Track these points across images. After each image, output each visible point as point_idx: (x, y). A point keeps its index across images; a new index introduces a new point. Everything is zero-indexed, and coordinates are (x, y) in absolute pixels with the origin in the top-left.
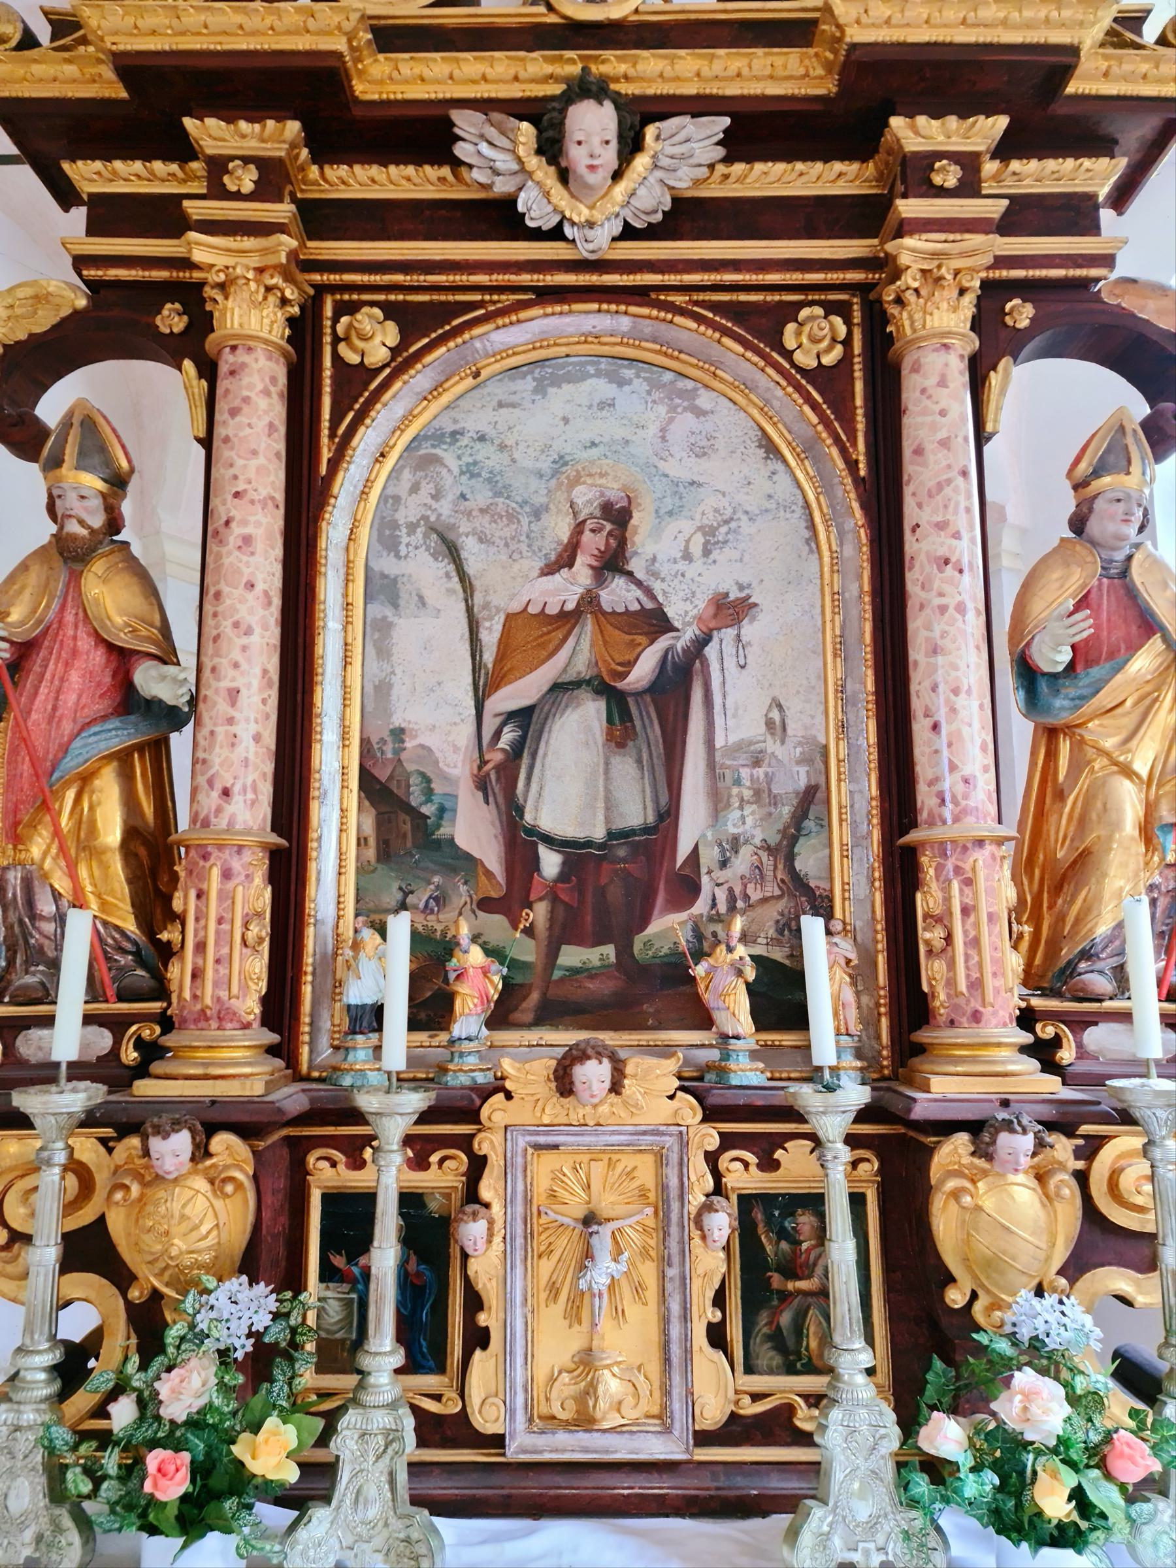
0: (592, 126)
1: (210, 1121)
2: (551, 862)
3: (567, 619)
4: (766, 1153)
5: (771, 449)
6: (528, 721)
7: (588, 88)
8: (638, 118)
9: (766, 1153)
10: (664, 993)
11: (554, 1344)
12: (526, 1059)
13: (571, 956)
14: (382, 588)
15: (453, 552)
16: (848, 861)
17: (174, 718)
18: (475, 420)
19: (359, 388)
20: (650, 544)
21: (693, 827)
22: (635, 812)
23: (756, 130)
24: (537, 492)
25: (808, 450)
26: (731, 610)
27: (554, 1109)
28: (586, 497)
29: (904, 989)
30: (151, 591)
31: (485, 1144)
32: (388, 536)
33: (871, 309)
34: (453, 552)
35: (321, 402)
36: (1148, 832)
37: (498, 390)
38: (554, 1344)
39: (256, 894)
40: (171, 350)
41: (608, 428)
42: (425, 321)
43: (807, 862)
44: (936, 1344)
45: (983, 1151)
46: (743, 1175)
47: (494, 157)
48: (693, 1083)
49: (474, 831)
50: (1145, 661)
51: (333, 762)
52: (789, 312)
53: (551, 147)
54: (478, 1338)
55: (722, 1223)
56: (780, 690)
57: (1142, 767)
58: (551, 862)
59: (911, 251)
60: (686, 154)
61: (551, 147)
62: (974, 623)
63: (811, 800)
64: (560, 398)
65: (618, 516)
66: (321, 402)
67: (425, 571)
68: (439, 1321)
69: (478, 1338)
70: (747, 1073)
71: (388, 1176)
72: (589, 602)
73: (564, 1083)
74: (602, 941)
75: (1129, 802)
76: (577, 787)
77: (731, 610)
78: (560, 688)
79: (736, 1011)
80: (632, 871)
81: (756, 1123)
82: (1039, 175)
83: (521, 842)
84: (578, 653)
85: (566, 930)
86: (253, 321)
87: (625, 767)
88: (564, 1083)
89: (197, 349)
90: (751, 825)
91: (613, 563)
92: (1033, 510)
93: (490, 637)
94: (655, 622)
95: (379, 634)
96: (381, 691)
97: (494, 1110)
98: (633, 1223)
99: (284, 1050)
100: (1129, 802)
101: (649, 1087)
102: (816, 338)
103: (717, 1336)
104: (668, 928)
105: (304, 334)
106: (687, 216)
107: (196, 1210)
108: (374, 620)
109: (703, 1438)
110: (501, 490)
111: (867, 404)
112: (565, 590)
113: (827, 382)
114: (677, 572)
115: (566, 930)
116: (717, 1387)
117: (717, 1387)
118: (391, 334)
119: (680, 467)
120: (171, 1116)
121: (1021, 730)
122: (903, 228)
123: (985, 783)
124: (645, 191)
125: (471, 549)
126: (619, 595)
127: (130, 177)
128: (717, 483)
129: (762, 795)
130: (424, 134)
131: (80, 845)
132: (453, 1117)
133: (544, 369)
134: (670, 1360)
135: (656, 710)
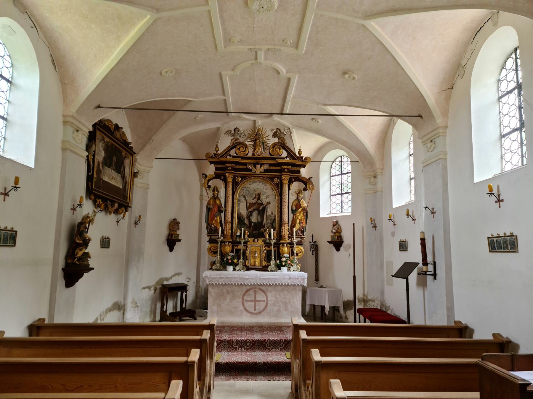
0: (258, 166)
1: (229, 242)
2: (253, 224)
3: (255, 204)
4: (269, 247)
5: (272, 189)
6: (251, 213)
7: (258, 164)
8: (261, 165)
9: (269, 247)
10: (262, 235)
11: (252, 261)
12: (251, 240)
13: (254, 232)
14: (239, 200)
15: (245, 197)
16: (277, 226)
17: (222, 212)
18: (247, 186)
19: (237, 183)
20: (263, 197)
21: (265, 222)
22: (260, 220)
23: (271, 165)
24: (252, 192)
25: (275, 190)
26: (269, 203)
27: (253, 243)
28: (256, 193)
29: (109, 135)
30: (220, 201)
31: (248, 245)
32: (239, 196)
33: (280, 178)
34: (245, 197)
35: (235, 185)
36: (299, 223)
37: (249, 183)
38: (252, 261)
39: (230, 226)
40: (223, 180)
41: (258, 187)
42: (243, 178)
43: (274, 225)
44: (279, 256)
45: (283, 245)
46: (267, 248)
47: (249, 167)
48: (263, 241)
49: (246, 221)
50: (300, 210)
51: (235, 215)
52: (274, 178)
53: (255, 167)
54: (247, 259)
55: (265, 251)
56: (271, 210)
57: (299, 218)
58: (253, 224)
59: (283, 177)
60: (266, 167)
61: (255, 167)
62: (287, 207)
63: (275, 220)
64: (255, 184)
65: (259, 195)
66: (235, 185)
67: (242, 199)
68: (245, 258)
69: (247, 259)
70: (268, 241)
71: (241, 247)
72: (257, 202)
73: (254, 241)
74: (257, 231)
75: (298, 221)
76: (255, 218)
77: (269, 203)
78: (254, 210)
79: (267, 236)
80: (259, 225)
81: (268, 244)
82: (294, 168)
83: (250, 222)
84: (255, 207)
85: (254, 230)
86: (230, 180)
87: (259, 217)
88: (254, 241)
89: (225, 180)
90: (269, 221)
91: (259, 199)
92: (293, 198)
93: (248, 205)
94: (262, 204)
95: (239, 204)
96: (239, 210)
97: (248, 243)
98: (258, 251)
99: (232, 238)
100: (298, 221)
101: (261, 242)
102: (276, 181)
103: (265, 260)
104: (263, 230)
105: (233, 180)
106: (266, 171)
107: (228, 249)
108: (358, 309)
109: (263, 267)
110: (249, 192)
111: (279, 188)
112: (254, 201)
113: (277, 184)
114: (264, 200)
115: (254, 230)
116: (264, 263)
117: (264, 263)
118: (240, 179)
119: (265, 190)
120: (227, 242)
121: (291, 216)
122: (282, 175)
123: (287, 219)
124: (262, 169)
125: (247, 197)
126: (259, 202)
127: (220, 166)
128: (267, 193)
129: (270, 219)
130: (245, 164)
131: (216, 222)
132: (246, 243)
133: (254, 182)
134: (261, 262)
135: (262, 212)
